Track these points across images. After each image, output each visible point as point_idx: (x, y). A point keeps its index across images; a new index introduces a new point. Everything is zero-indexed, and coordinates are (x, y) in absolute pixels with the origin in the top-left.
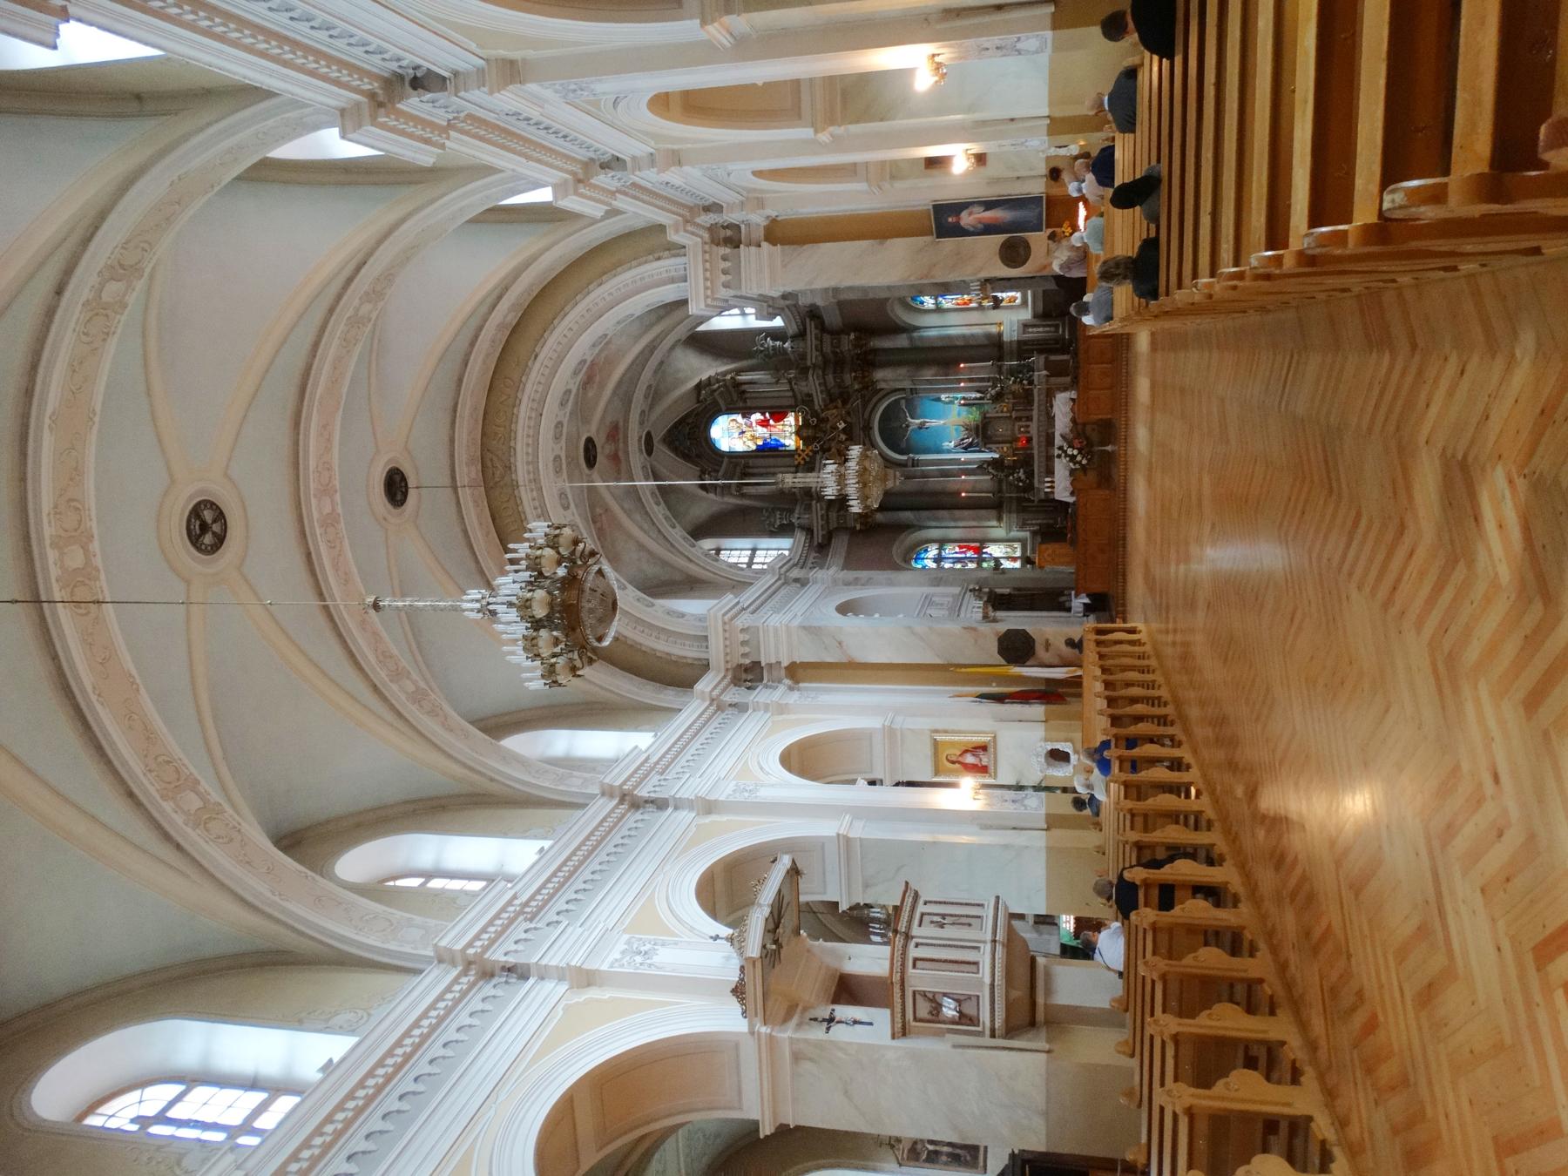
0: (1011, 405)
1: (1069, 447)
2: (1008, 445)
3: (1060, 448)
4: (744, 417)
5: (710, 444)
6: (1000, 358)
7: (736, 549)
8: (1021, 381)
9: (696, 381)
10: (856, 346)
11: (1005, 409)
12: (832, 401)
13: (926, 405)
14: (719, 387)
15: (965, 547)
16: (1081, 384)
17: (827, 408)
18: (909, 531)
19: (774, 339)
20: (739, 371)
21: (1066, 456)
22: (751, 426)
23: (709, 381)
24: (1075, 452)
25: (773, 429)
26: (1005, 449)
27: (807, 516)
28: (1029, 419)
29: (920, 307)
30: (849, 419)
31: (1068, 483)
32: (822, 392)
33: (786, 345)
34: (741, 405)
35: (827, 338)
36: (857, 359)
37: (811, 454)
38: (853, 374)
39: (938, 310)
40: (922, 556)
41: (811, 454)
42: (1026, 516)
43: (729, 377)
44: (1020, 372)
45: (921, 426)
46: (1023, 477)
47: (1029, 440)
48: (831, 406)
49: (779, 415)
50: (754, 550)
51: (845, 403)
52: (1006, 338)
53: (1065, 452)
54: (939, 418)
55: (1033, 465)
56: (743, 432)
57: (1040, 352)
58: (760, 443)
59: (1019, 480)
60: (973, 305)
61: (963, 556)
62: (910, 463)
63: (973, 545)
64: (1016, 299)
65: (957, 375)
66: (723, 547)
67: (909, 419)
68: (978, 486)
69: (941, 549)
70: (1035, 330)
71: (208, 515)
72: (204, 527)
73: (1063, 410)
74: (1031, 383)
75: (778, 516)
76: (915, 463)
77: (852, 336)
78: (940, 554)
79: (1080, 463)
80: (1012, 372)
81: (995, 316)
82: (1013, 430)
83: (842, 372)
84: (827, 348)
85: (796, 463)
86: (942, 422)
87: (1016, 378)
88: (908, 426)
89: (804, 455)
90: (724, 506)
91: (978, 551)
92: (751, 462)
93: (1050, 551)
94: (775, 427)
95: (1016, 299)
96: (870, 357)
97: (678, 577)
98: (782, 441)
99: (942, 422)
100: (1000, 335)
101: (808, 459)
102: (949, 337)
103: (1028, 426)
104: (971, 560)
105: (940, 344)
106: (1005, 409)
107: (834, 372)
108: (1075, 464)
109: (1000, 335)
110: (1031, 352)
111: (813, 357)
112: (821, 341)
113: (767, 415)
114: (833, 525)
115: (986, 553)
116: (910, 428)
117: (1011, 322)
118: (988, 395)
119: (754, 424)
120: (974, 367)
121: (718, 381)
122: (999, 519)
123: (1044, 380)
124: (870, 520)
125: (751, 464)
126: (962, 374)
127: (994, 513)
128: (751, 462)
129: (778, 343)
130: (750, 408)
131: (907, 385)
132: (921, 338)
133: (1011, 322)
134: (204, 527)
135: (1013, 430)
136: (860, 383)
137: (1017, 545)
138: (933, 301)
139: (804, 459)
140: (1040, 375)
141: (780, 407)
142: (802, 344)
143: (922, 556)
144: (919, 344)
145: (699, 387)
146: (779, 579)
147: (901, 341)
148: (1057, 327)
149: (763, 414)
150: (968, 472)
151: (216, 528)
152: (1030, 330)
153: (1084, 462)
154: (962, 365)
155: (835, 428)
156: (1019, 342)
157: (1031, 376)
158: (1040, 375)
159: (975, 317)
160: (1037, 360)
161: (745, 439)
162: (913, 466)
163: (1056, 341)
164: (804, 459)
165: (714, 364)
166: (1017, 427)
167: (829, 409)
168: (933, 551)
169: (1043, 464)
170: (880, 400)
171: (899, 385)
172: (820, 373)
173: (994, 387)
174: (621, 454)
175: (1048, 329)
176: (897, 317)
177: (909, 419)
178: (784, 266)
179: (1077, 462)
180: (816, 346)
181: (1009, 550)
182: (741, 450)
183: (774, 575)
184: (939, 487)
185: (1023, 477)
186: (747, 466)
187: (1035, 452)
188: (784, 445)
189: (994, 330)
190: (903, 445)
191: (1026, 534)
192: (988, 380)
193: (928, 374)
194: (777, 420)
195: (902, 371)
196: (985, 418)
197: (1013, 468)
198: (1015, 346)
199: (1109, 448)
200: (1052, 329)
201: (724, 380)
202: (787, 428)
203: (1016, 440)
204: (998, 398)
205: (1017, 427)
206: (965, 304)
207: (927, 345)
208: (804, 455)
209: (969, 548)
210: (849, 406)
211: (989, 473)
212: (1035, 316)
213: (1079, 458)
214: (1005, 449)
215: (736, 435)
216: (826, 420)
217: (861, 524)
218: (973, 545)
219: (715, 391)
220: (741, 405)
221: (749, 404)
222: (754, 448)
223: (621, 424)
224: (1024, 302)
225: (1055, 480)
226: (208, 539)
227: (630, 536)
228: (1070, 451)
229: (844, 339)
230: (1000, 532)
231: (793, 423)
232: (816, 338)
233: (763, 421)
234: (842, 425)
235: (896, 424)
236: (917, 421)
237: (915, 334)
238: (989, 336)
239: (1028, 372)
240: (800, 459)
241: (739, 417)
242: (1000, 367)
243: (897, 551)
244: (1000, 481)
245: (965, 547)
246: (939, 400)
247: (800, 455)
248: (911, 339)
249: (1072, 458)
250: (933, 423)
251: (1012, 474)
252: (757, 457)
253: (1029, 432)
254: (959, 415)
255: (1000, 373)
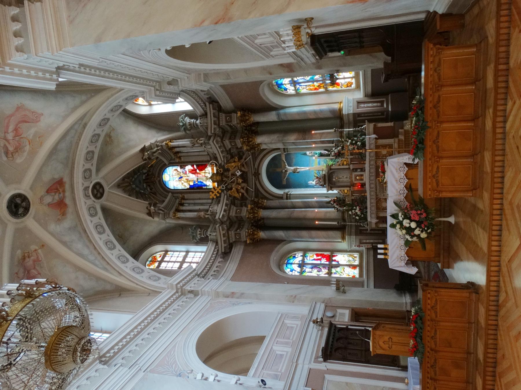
0: (349, 160)
1: (406, 217)
2: (348, 189)
3: (395, 216)
4: (181, 168)
5: (163, 184)
6: (342, 127)
7: (177, 251)
8: (356, 142)
9: (142, 146)
10: (241, 121)
11: (345, 163)
12: (232, 157)
13: (298, 157)
14: (158, 150)
15: (321, 255)
16: (429, 150)
17: (228, 162)
18: (283, 243)
19: (191, 118)
20: (171, 140)
21: (402, 227)
22: (186, 173)
23: (150, 147)
24: (413, 225)
25: (199, 175)
26: (346, 191)
27: (214, 234)
28: (363, 170)
29: (284, 92)
30: (243, 169)
31: (403, 253)
32: (222, 152)
33: (198, 122)
34: (177, 160)
35: (223, 116)
36: (246, 130)
37: (220, 192)
38: (241, 140)
39: (298, 94)
40: (291, 261)
41: (220, 192)
42: (361, 237)
43: (164, 144)
44: (356, 136)
45: (295, 171)
46: (359, 213)
47: (363, 185)
48: (232, 160)
49: (202, 167)
50: (187, 252)
51: (240, 158)
52: (345, 112)
53: (401, 223)
54: (307, 166)
55: (366, 202)
56: (181, 177)
57: (370, 121)
58: (192, 184)
59: (356, 214)
60: (322, 90)
61: (319, 262)
62: (285, 197)
63: (326, 253)
64: (352, 83)
65: (311, 139)
66: (169, 250)
67: (287, 167)
68: (328, 216)
69: (304, 256)
70: (366, 105)
71: (18, 201)
72: (17, 206)
73: (397, 175)
74: (364, 145)
75: (198, 233)
76: (288, 197)
77: (239, 114)
78: (303, 260)
79: (418, 236)
80: (349, 136)
81: (336, 97)
82: (351, 178)
83: (235, 139)
84: (223, 123)
85: (211, 197)
86: (308, 168)
87: (352, 140)
88: (286, 171)
89: (216, 192)
90: (167, 224)
91: (329, 258)
92: (186, 196)
93: (386, 338)
94: (199, 174)
95: (352, 83)
96: (253, 128)
97: (108, 287)
98: (205, 182)
99: (308, 168)
100: (340, 110)
101: (218, 195)
102: (305, 113)
103: (362, 175)
104: (324, 266)
105: (297, 118)
106: (345, 163)
107: (230, 138)
108: (412, 237)
109: (340, 110)
110: (363, 122)
111: (212, 129)
112: (219, 118)
113: (195, 166)
114: (233, 239)
115: (335, 261)
116: (288, 173)
117: (348, 101)
118: (333, 153)
119: (188, 172)
120: (323, 133)
121: (157, 146)
122: (343, 238)
123: (373, 142)
124: (255, 236)
125: (186, 198)
126: (315, 138)
127: (338, 234)
128: (186, 196)
129: (192, 120)
130: (184, 162)
131: (280, 146)
132: (285, 114)
133: (348, 101)
134: (17, 206)
135: (351, 178)
136: (247, 146)
137: (356, 255)
138: (293, 88)
139: (215, 195)
140: (370, 138)
141: (202, 161)
142: (205, 121)
143: (291, 261)
144: (285, 118)
145: (143, 150)
146: (177, 292)
147: (272, 117)
148: (382, 103)
149: (193, 166)
150: (321, 205)
151: (24, 204)
152: (362, 105)
153: (424, 235)
154: (313, 132)
155: (234, 175)
156: (354, 114)
157: (364, 139)
158: (370, 138)
159: (324, 98)
160: (369, 127)
161: (183, 182)
162: (287, 199)
163: (382, 113)
164: (215, 195)
165: (157, 135)
166: (353, 176)
167: (230, 163)
168: (299, 258)
169: (374, 204)
170: (264, 156)
171: (274, 146)
172: (219, 140)
173: (337, 146)
174: (68, 201)
175: (375, 104)
176: (268, 99)
177: (287, 167)
178: (71, 22)
179: (415, 235)
180: (214, 121)
181: (351, 259)
182: (181, 188)
183: (172, 289)
184: (301, 215)
185: (359, 213)
186: (183, 198)
187: (368, 194)
188: (206, 185)
189: (336, 106)
190: (284, 183)
191: (363, 248)
192: (332, 142)
193: (292, 138)
194: (201, 170)
195: (274, 137)
196: (331, 169)
197: (351, 206)
198: (351, 118)
199: (452, 220)
200: (379, 104)
201: (162, 146)
202: (207, 175)
203: (353, 185)
204: (339, 155)
205: (353, 176)
206: (316, 89)
207: (290, 118)
208: (216, 192)
209: (323, 256)
210: (242, 160)
211: (334, 207)
212: (366, 95)
213: (417, 232)
214: (346, 191)
215: (177, 179)
216: (228, 170)
217: (251, 239)
218: (326, 253)
219: (155, 152)
220: (177, 160)
221: (183, 160)
222: (188, 187)
223: (66, 179)
224: (358, 87)
225: (389, 247)
226: (21, 211)
227: (67, 262)
228: (406, 223)
229: (234, 115)
230: (344, 245)
231: (211, 171)
232: (214, 117)
233: (192, 170)
234: (239, 173)
235: (279, 170)
236: (292, 168)
237: (282, 111)
238: (333, 111)
239: (361, 136)
240: (213, 195)
241: (178, 168)
242: (341, 133)
243: (274, 257)
244: (343, 212)
245: (321, 255)
246: (305, 154)
247: (213, 192)
248: (278, 115)
249: (410, 231)
250: (302, 169)
251: (351, 210)
252: (190, 193)
253: (362, 180)
254: (319, 164)
255: (341, 137)
